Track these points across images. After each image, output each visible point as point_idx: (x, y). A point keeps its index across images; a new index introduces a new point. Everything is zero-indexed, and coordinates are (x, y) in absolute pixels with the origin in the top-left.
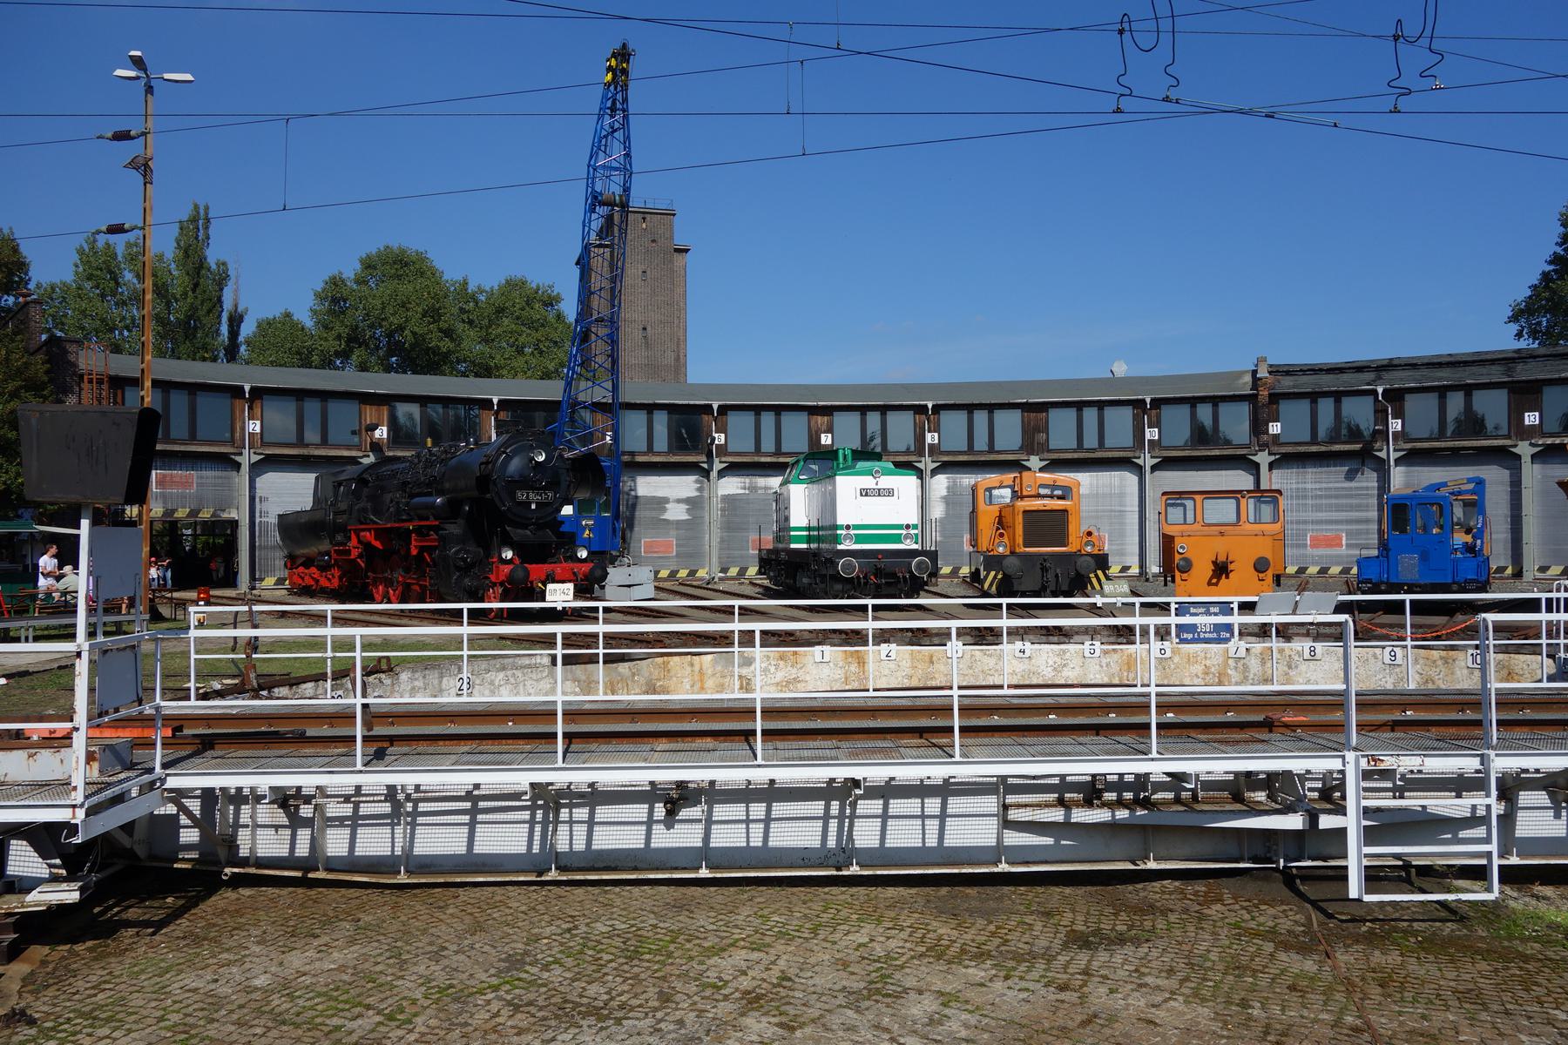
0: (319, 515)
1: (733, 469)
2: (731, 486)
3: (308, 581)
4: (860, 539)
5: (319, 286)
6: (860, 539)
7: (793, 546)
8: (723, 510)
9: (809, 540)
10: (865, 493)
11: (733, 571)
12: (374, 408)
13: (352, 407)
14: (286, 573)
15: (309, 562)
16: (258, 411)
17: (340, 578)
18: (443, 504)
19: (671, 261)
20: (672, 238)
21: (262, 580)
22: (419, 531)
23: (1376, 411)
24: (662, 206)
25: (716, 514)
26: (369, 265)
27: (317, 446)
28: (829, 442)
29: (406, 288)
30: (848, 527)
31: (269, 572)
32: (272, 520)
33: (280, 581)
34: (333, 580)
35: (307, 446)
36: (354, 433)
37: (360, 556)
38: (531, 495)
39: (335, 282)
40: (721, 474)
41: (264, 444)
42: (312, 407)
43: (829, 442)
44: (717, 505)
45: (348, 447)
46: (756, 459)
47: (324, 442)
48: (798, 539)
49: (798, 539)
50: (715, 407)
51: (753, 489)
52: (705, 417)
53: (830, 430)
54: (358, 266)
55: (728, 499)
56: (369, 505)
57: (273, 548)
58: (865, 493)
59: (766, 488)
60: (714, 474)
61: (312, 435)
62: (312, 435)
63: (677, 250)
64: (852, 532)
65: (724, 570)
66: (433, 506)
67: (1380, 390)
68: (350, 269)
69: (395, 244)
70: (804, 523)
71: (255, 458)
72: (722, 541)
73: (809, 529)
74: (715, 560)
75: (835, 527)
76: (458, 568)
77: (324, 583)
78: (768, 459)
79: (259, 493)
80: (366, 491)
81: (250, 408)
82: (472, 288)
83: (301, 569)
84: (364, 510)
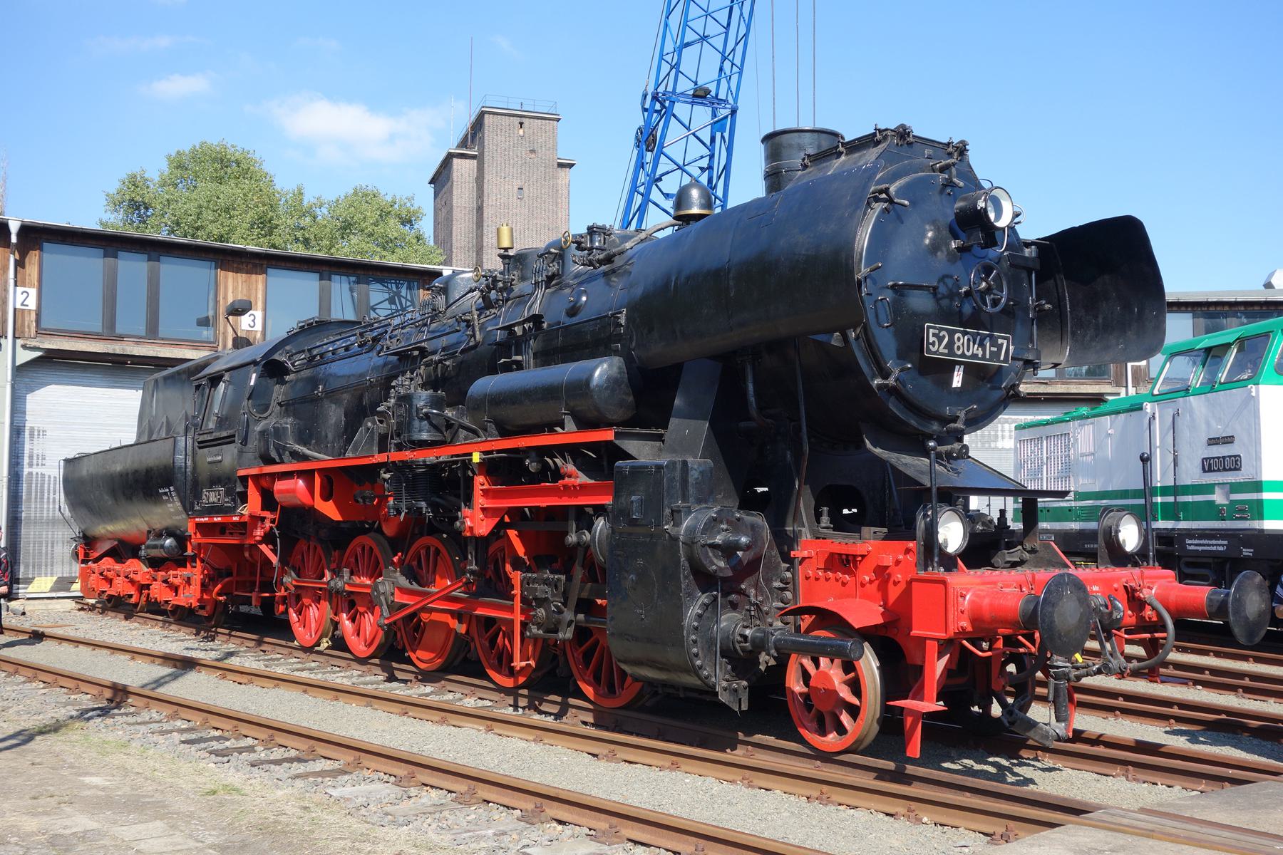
0: (155, 455)
3: (120, 587)
5: (113, 187)
12: (241, 277)
13: (198, 272)
14: (76, 568)
15: (124, 550)
16: (32, 269)
17: (204, 587)
18: (613, 383)
19: (554, 177)
20: (555, 148)
21: (29, 581)
22: (505, 469)
24: (543, 108)
26: (179, 165)
27: (139, 339)
29: (228, 191)
31: (44, 566)
32: (53, 471)
33: (63, 584)
34: (188, 585)
35: (121, 338)
36: (204, 322)
37: (268, 538)
38: (961, 341)
39: (134, 182)
41: (41, 331)
42: (132, 268)
45: (195, 344)
47: (152, 333)
54: (164, 166)
56: (288, 423)
57: (53, 522)
61: (131, 316)
62: (131, 316)
63: (561, 165)
66: (581, 387)
68: (155, 169)
69: (214, 140)
71: (25, 356)
75: (1257, 486)
76: (705, 580)
77: (158, 592)
79: (31, 421)
80: (279, 392)
81: (20, 264)
82: (308, 199)
83: (107, 563)
84: (278, 432)
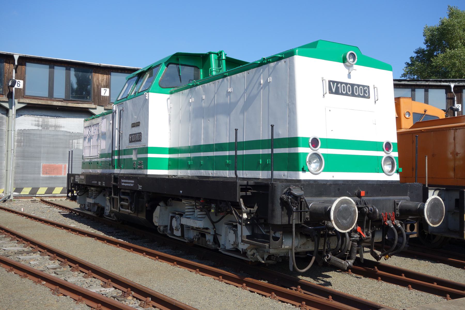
1: (31, 108)
2: (28, 122)
4: (333, 163)
6: (333, 163)
7: (150, 172)
8: (19, 141)
9: (173, 164)
10: (336, 88)
11: (26, 191)
23: (447, 98)
25: (13, 145)
28: (107, 94)
30: (315, 143)
40: (19, 112)
43: (107, 94)
44: (13, 137)
46: (49, 103)
48: (158, 164)
49: (158, 164)
50: (16, 57)
51: (45, 126)
52: (7, 66)
53: (107, 86)
55: (22, 133)
58: (336, 88)
59: (56, 126)
60: (13, 112)
64: (321, 151)
65: (18, 190)
67: (452, 85)
70: (167, 145)
72: (17, 166)
73: (172, 151)
74: (11, 182)
75: (294, 142)
78: (59, 104)
